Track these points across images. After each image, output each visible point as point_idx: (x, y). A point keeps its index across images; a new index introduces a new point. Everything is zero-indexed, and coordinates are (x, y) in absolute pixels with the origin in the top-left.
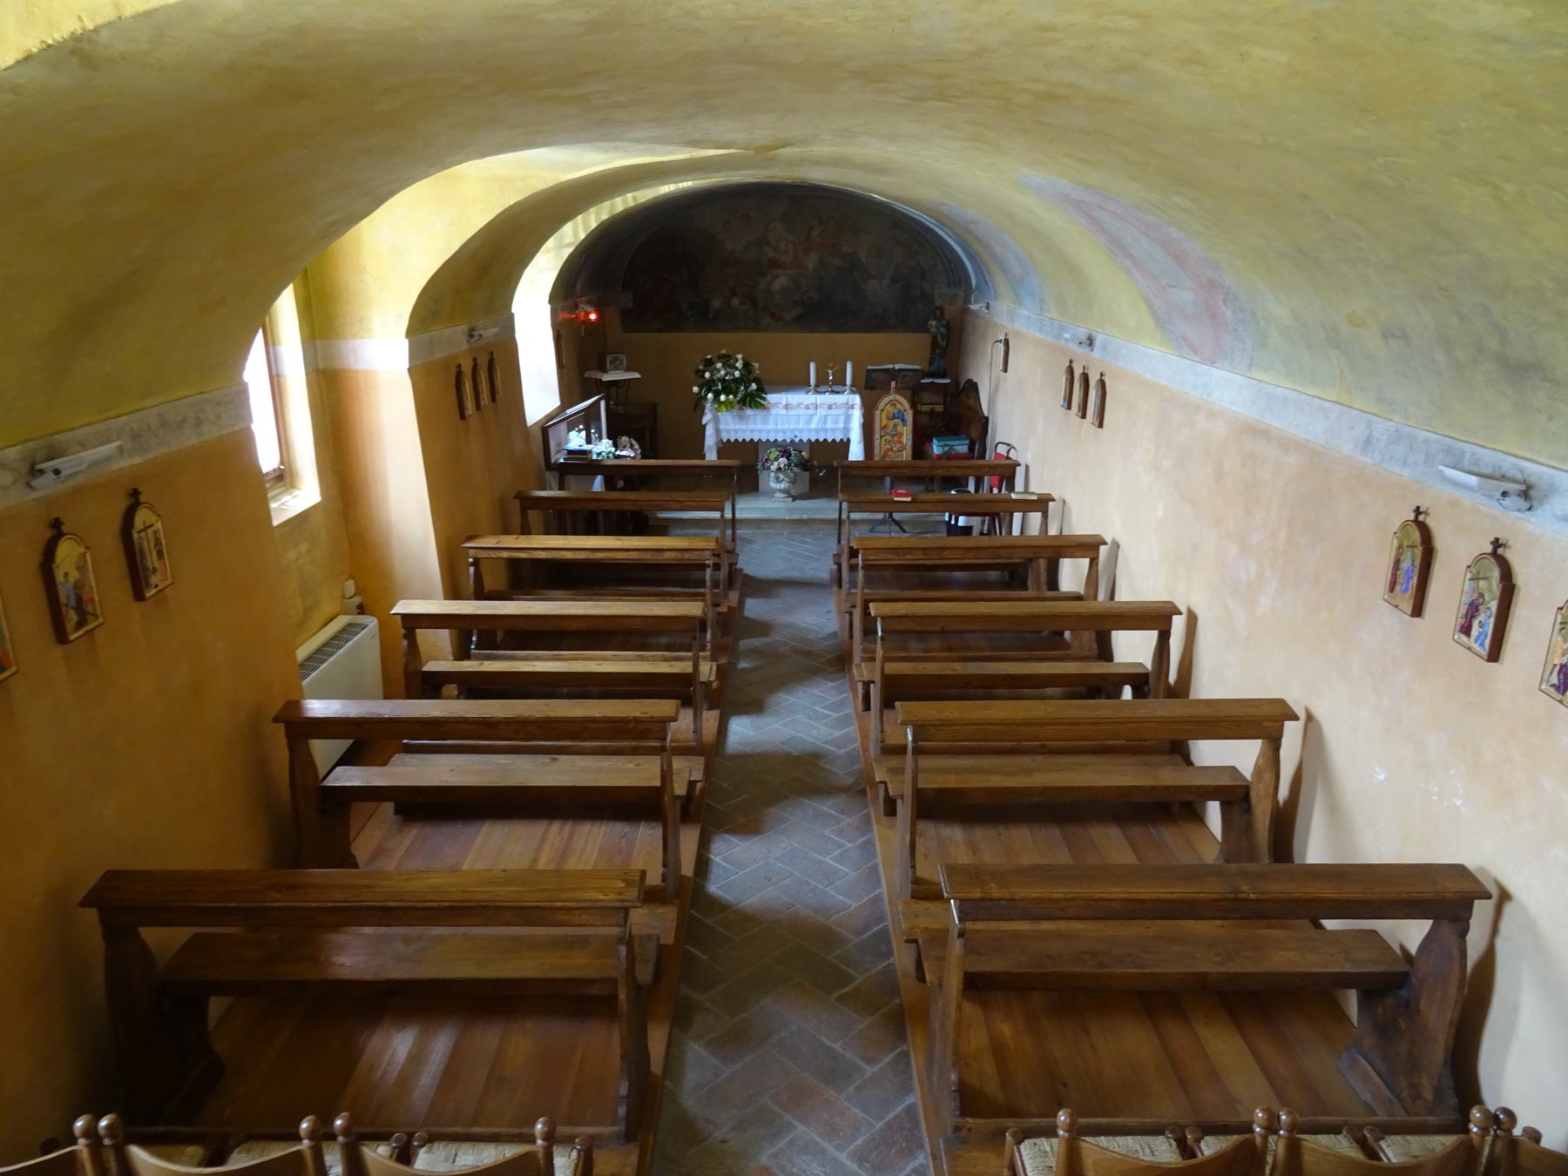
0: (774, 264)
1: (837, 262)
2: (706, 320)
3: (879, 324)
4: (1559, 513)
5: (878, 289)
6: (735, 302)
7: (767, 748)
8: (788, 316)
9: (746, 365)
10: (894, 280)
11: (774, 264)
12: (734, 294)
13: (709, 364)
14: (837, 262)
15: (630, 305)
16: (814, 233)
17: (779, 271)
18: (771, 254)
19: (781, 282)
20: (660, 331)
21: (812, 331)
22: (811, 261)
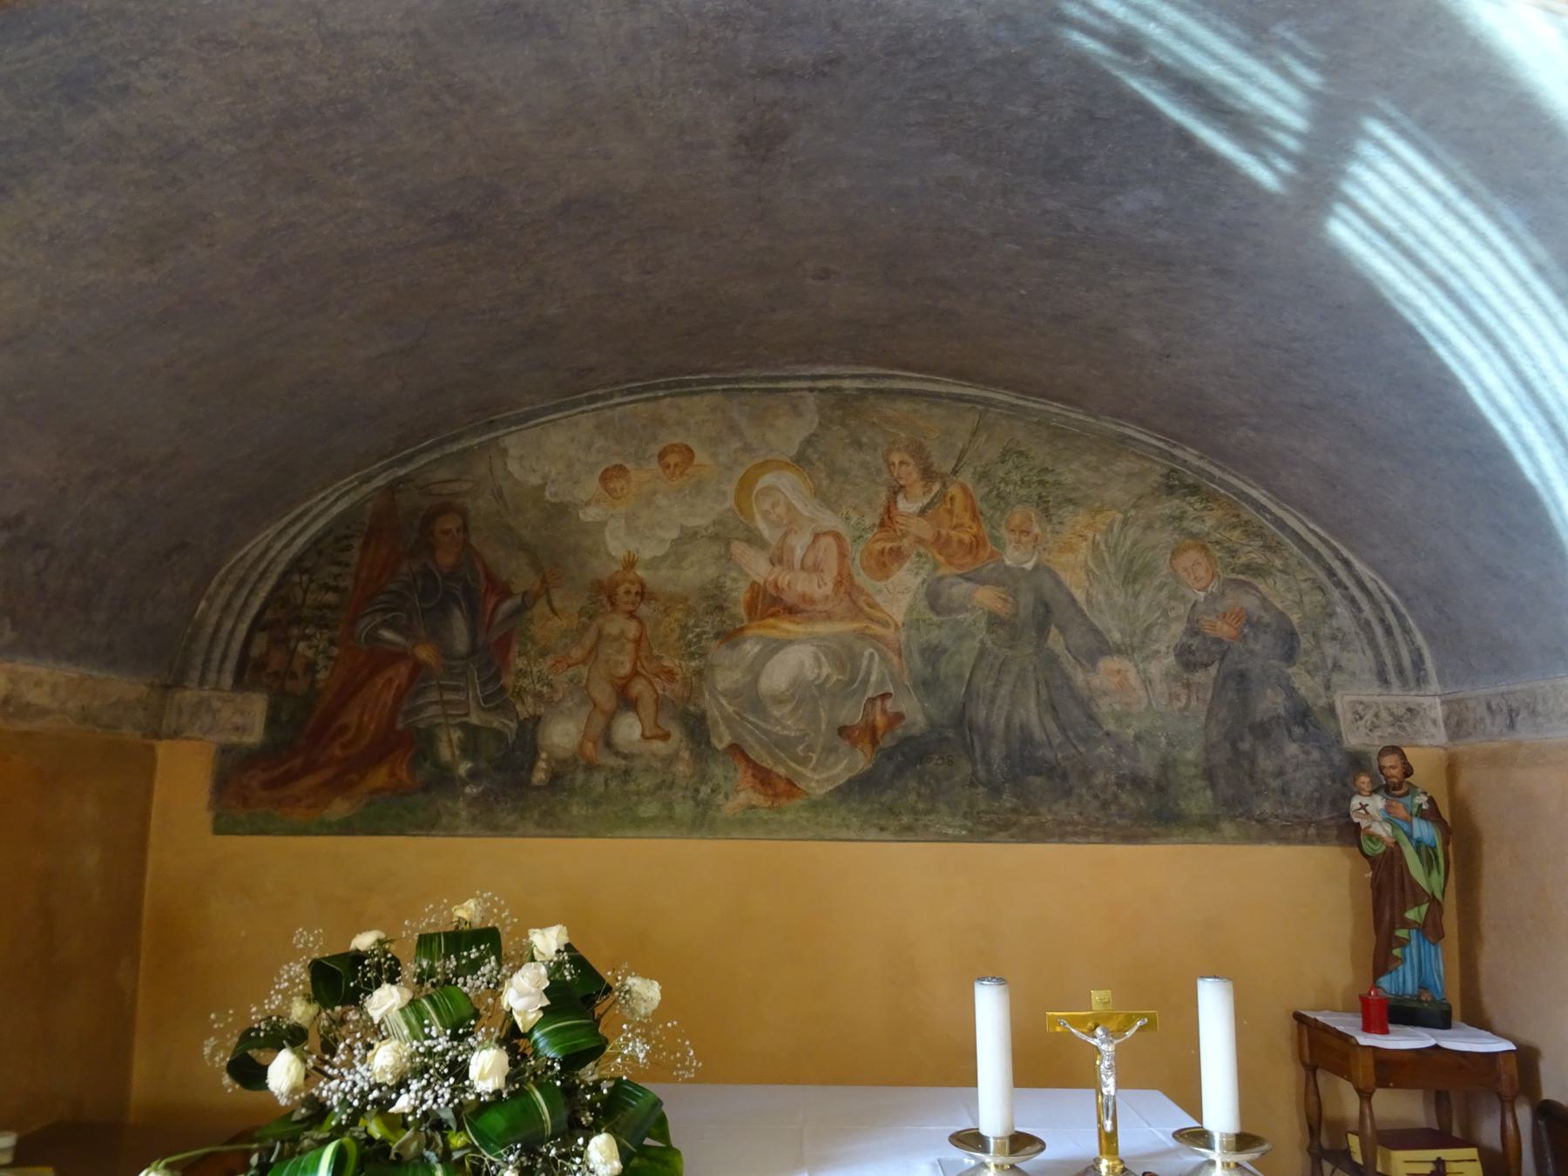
0: (770, 604)
1: (987, 597)
2: (517, 785)
3: (1149, 808)
4: (819, 792)
5: (1139, 694)
6: (629, 730)
7: (1469, 21)
8: (818, 781)
9: (578, 993)
10: (1188, 659)
11: (770, 604)
12: (627, 702)
13: (340, 981)
14: (987, 597)
15: (255, 736)
16: (903, 505)
17: (788, 627)
18: (759, 568)
19: (793, 662)
20: (346, 828)
21: (908, 832)
22: (899, 594)
